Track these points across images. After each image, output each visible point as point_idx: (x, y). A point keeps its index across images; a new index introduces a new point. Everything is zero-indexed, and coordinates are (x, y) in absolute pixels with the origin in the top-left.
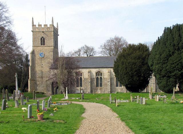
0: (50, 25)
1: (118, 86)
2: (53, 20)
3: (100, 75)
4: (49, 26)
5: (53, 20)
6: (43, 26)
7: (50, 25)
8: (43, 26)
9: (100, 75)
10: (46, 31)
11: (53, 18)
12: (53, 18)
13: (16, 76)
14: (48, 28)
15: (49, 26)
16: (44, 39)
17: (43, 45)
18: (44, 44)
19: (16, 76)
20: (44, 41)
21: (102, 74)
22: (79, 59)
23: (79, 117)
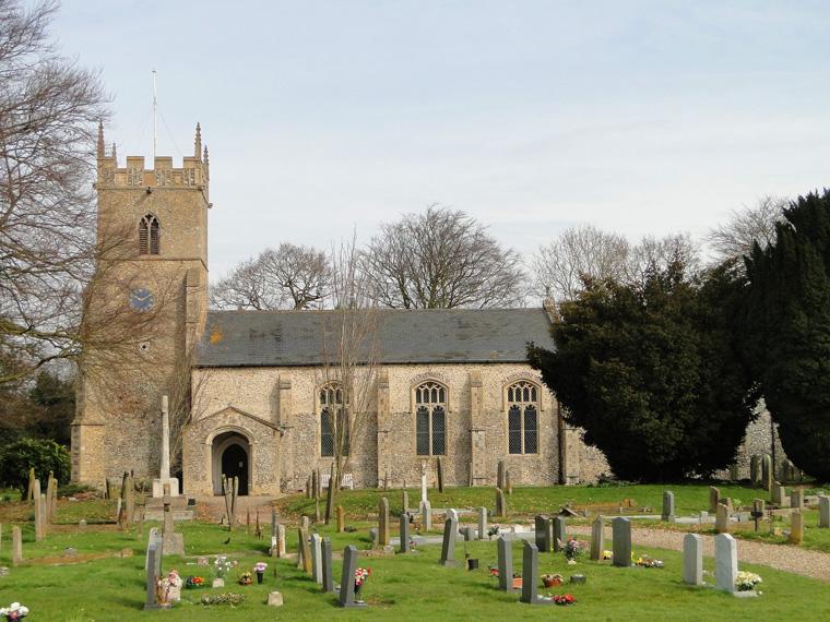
0: (186, 160)
1: (428, 454)
2: (198, 135)
3: (526, 399)
4: (178, 164)
5: (198, 135)
6: (149, 165)
7: (186, 160)
8: (149, 165)
9: (526, 399)
10: (167, 185)
11: (198, 129)
12: (198, 129)
13: (15, 606)
14: (177, 172)
15: (178, 164)
16: (155, 224)
17: (152, 253)
18: (155, 250)
19: (15, 606)
20: (154, 234)
21: (442, 392)
22: (12, 543)
23: (13, 111)
